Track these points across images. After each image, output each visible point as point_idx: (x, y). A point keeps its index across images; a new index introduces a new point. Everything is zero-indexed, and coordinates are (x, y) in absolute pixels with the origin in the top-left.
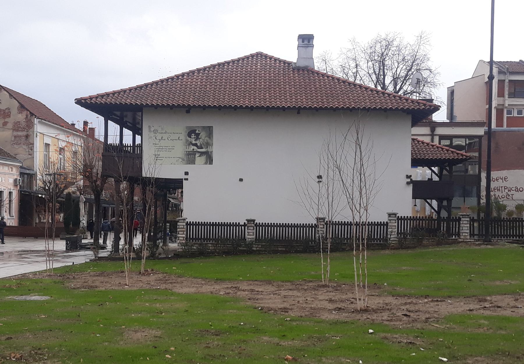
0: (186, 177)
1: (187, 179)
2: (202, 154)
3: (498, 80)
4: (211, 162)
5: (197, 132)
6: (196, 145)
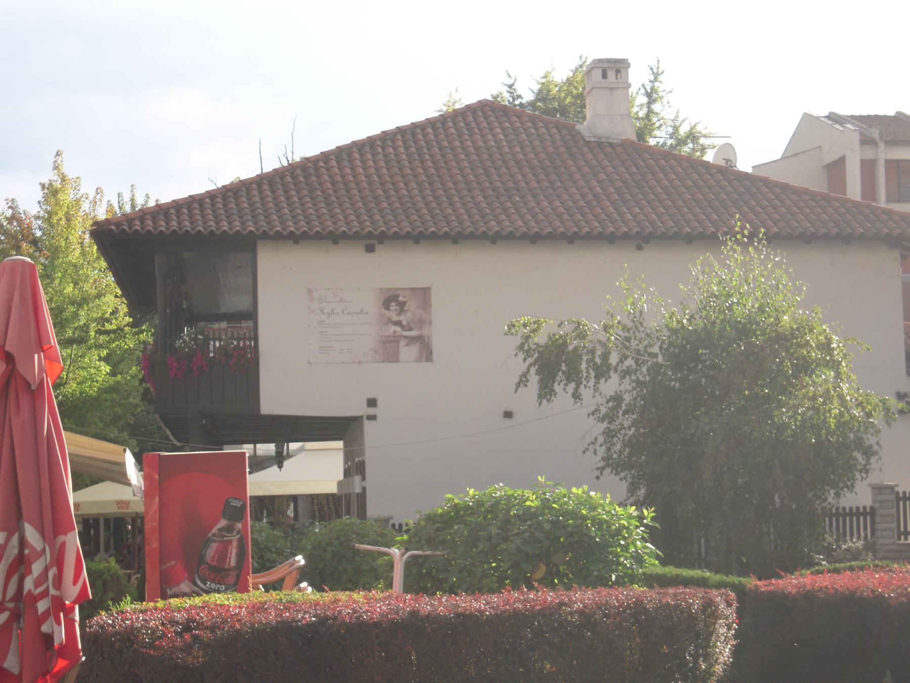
0: (372, 411)
1: (372, 418)
2: (411, 340)
3: (903, 283)
4: (429, 359)
5: (401, 299)
6: (398, 323)
